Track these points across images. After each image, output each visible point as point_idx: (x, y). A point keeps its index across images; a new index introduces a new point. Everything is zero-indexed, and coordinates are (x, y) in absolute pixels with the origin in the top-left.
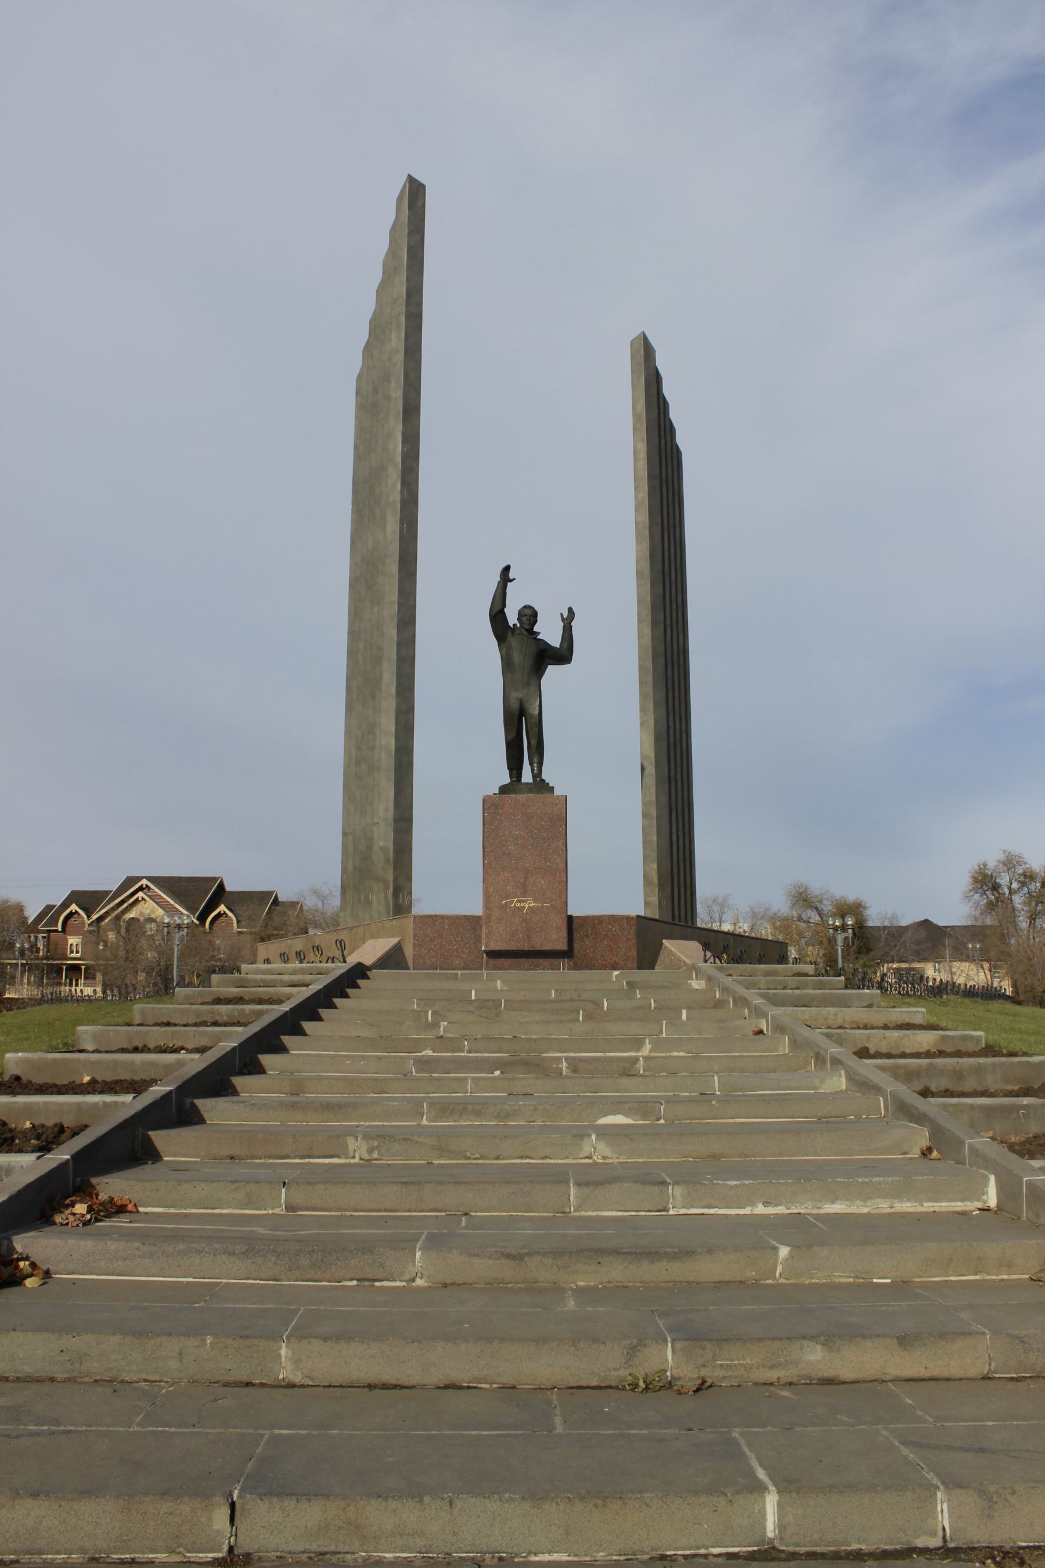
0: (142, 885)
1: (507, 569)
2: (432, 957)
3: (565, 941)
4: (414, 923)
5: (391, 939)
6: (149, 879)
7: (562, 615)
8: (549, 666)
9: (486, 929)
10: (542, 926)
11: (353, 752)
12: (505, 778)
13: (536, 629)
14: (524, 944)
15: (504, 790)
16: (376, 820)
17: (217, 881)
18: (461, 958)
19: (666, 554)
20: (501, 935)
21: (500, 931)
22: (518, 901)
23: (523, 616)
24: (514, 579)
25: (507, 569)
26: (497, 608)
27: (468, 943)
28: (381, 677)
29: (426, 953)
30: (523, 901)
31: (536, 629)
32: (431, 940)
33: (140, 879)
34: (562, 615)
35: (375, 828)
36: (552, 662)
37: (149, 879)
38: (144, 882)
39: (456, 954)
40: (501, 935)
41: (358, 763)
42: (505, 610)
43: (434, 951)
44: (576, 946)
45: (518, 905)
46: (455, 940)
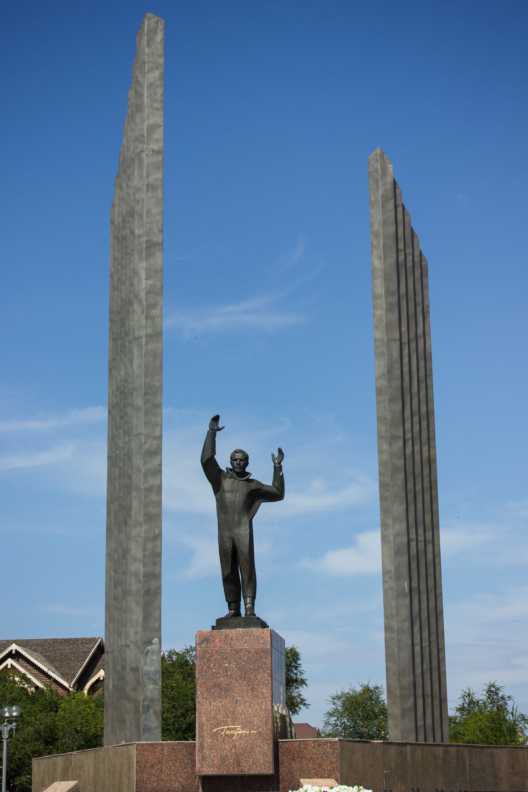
0: (11, 651)
1: (216, 419)
2: (153, 782)
3: (272, 766)
4: (137, 750)
5: (71, 782)
6: (18, 643)
7: (273, 456)
8: (263, 504)
9: (199, 755)
10: (250, 752)
11: (112, 573)
12: (224, 610)
13: (247, 470)
14: (234, 769)
15: (221, 624)
16: (129, 643)
17: (96, 642)
18: (179, 782)
19: (406, 369)
20: (213, 760)
21: (212, 758)
22: (228, 729)
23: (234, 460)
24: (224, 427)
25: (216, 419)
26: (208, 456)
27: (185, 768)
28: (131, 505)
29: (148, 778)
30: (232, 729)
31: (247, 470)
32: (152, 766)
33: (9, 643)
34: (273, 456)
35: (128, 650)
36: (264, 500)
37: (18, 643)
38: (14, 647)
39: (174, 778)
40: (213, 760)
41: (115, 586)
42: (215, 456)
43: (154, 776)
44: (282, 769)
45: (228, 732)
46: (174, 765)
